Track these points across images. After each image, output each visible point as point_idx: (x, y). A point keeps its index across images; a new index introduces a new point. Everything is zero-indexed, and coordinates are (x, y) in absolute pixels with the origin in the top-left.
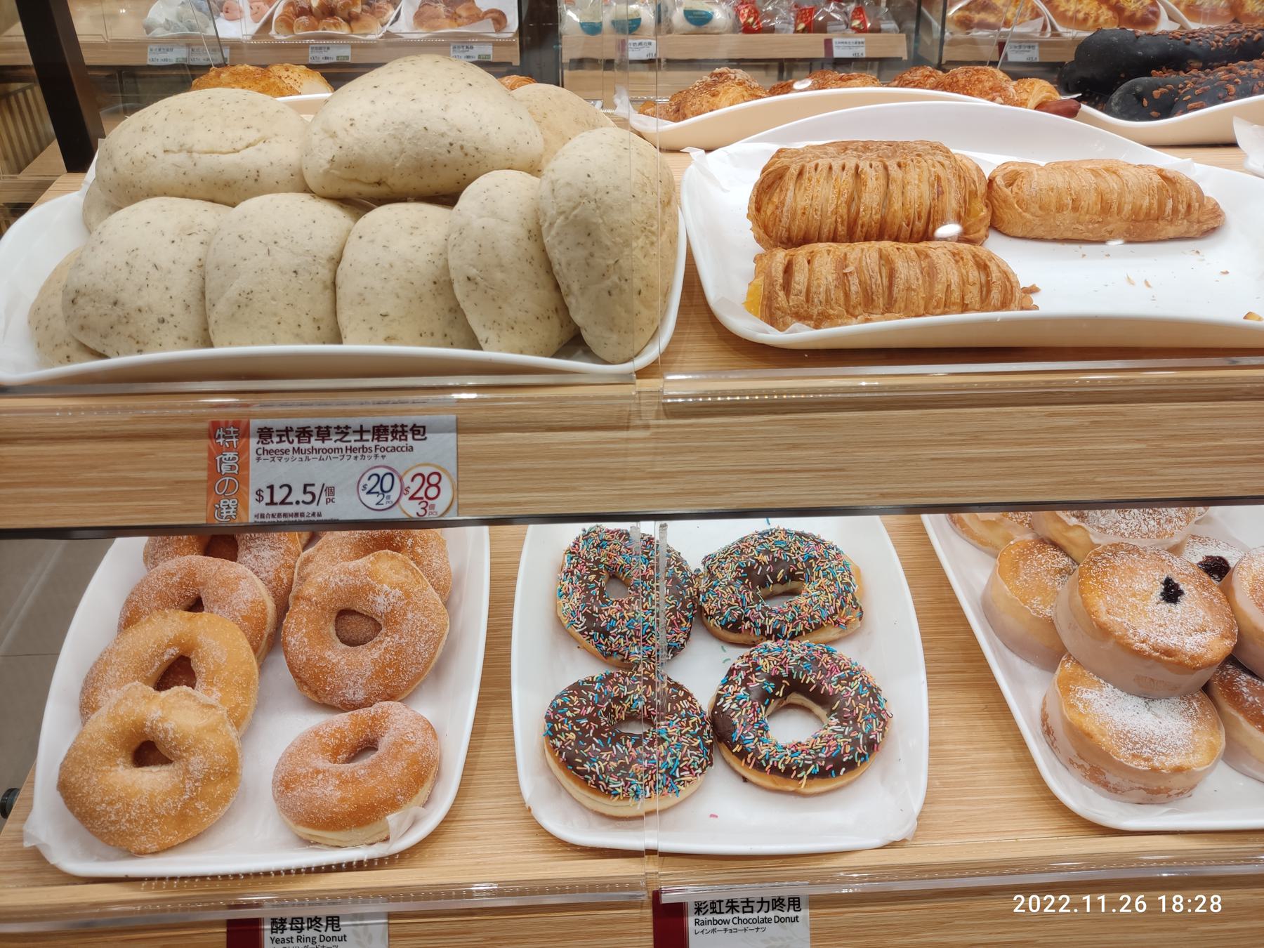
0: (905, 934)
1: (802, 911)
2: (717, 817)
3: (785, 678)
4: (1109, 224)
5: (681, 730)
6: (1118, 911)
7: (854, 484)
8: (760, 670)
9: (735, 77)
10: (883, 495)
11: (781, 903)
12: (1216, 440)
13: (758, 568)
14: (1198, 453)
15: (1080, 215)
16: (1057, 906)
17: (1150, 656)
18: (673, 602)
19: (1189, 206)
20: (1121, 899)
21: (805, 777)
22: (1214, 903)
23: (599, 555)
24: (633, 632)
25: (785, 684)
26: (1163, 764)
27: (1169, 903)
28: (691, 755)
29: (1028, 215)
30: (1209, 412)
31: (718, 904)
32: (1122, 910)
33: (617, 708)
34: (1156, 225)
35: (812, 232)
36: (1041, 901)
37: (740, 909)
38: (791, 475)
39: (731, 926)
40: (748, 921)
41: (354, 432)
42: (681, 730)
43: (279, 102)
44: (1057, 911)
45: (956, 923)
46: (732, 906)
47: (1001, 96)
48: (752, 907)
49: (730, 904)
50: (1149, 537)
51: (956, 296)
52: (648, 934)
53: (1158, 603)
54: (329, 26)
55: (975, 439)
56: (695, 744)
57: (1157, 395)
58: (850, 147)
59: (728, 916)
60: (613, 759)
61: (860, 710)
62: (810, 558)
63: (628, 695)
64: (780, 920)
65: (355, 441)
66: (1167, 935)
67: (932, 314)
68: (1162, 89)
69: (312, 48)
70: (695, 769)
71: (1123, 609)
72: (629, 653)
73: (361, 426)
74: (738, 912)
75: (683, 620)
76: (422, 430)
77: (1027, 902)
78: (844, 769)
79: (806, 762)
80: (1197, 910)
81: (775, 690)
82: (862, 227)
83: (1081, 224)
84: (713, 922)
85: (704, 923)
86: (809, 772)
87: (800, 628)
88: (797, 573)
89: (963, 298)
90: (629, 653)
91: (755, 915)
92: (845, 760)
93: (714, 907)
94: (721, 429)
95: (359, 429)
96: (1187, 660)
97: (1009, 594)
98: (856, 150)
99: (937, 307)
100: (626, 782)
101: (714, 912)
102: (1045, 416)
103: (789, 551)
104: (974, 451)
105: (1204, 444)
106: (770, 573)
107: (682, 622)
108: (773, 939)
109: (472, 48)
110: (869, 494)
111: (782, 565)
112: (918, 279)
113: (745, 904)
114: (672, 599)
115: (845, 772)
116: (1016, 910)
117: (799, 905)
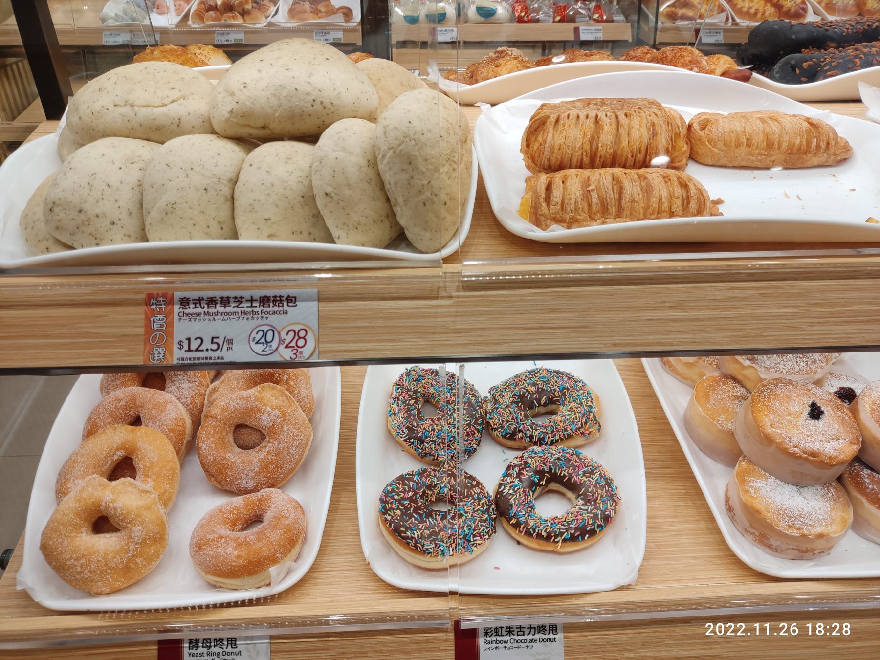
0: (630, 651)
1: (558, 634)
2: (499, 568)
3: (547, 472)
4: (772, 156)
5: (474, 509)
6: (778, 634)
7: (594, 337)
8: (529, 467)
9: (512, 54)
10: (615, 345)
11: (544, 629)
12: (846, 306)
13: (528, 395)
14: (834, 316)
15: (752, 150)
16: (736, 631)
17: (800, 457)
18: (468, 419)
19: (828, 144)
20: (781, 626)
21: (561, 541)
22: (845, 629)
23: (417, 386)
24: (441, 440)
25: (547, 476)
26: (810, 532)
27: (814, 629)
28: (481, 525)
29: (715, 150)
30: (842, 287)
31: (500, 629)
32: (781, 634)
33: (430, 493)
34: (805, 157)
35: (565, 161)
36: (725, 627)
37: (515, 633)
38: (551, 331)
39: (509, 645)
40: (521, 641)
41: (247, 301)
42: (474, 509)
43: (194, 71)
44: (736, 634)
45: (666, 642)
46: (510, 631)
47: (697, 67)
48: (524, 631)
49: (508, 630)
50: (800, 374)
51: (666, 206)
52: (451, 650)
53: (806, 420)
54: (229, 18)
55: (679, 305)
56: (484, 518)
57: (805, 275)
58: (592, 102)
59: (507, 638)
60: (426, 528)
61: (599, 494)
62: (564, 388)
63: (437, 484)
64: (543, 640)
65: (247, 307)
66: (812, 651)
67: (649, 219)
68: (809, 62)
69: (217, 33)
70: (484, 536)
71: (782, 424)
72: (438, 455)
73: (252, 297)
74: (514, 635)
75: (476, 431)
76: (294, 299)
77: (715, 628)
78: (587, 536)
79: (561, 530)
80: (834, 634)
81: (540, 480)
82: (600, 158)
83: (752, 156)
84: (497, 642)
85: (490, 643)
86: (563, 537)
87: (557, 437)
88: (555, 399)
89: (670, 208)
90: (438, 455)
91: (525, 637)
92: (588, 529)
93: (497, 631)
94: (502, 298)
95: (250, 298)
96: (826, 460)
97: (703, 413)
98: (596, 104)
99: (652, 214)
100: (436, 545)
101: (497, 635)
102: (728, 289)
103: (549, 384)
104: (678, 314)
105: (838, 309)
106: (536, 399)
107: (475, 433)
108: (538, 653)
109: (328, 33)
110: (605, 344)
111: (544, 393)
112: (639, 194)
113: (519, 630)
114: (468, 417)
115: (588, 538)
116: (707, 634)
117: (556, 630)
